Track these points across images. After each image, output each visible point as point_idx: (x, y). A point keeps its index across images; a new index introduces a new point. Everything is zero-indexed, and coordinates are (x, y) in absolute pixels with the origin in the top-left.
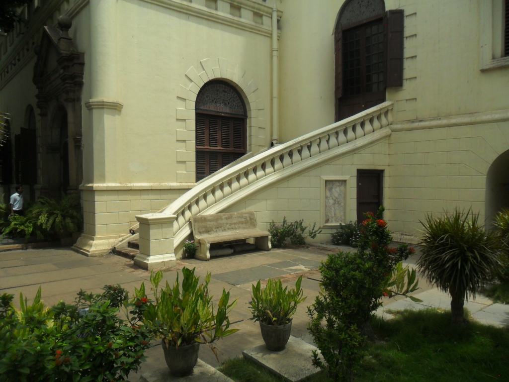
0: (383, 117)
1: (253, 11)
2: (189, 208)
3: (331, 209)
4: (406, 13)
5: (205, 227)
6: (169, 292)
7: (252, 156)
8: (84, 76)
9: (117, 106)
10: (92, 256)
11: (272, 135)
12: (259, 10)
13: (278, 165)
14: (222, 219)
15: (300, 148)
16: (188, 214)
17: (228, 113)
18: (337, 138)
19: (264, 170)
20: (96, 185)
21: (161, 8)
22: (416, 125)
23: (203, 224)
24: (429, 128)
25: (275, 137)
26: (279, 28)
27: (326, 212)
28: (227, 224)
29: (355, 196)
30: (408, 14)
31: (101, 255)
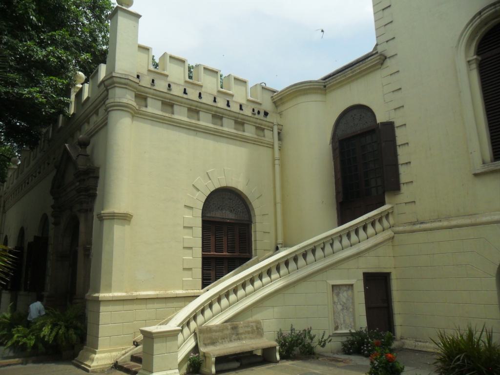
2: (195, 318)
4: (396, 125)
8: (98, 188)
9: (127, 217)
11: (276, 239)
13: (283, 270)
17: (234, 220)
18: (341, 242)
22: (417, 227)
24: (431, 230)
26: (280, 139)
27: (334, 319)
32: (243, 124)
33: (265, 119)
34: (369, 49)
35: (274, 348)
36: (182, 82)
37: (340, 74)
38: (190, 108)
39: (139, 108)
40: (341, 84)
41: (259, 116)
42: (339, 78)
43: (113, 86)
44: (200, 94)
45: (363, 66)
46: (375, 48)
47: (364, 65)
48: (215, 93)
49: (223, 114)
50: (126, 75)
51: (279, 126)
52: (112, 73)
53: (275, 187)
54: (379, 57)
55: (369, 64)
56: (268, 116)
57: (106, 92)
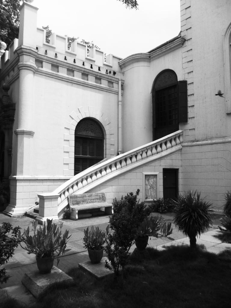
0: (177, 140)
1: (108, 81)
2: (68, 190)
3: (149, 191)
4: (188, 83)
5: (76, 201)
6: (41, 231)
7: (107, 160)
8: (15, 116)
9: (31, 133)
10: (13, 217)
11: (118, 149)
12: (111, 80)
13: (119, 166)
14: (86, 197)
15: (131, 156)
16: (67, 194)
17: (94, 137)
18: (151, 151)
19: (111, 169)
20: (18, 177)
21: (58, 80)
22: (195, 143)
23: (75, 199)
25: (120, 150)
26: (122, 89)
27: (145, 193)
28: (89, 199)
29: (162, 184)
30: (189, 83)
31: (19, 217)
32: (100, 79)
33: (114, 76)
34: (176, 35)
35: (111, 207)
36: (64, 52)
37: (159, 49)
38: (69, 69)
39: (38, 68)
40: (159, 56)
41: (110, 74)
42: (158, 52)
43: (22, 54)
44: (75, 60)
45: (172, 45)
46: (180, 34)
47: (173, 44)
48: (84, 60)
49: (88, 73)
50: (29, 47)
51: (122, 81)
52: (21, 46)
53: (118, 118)
54: (181, 40)
55: (176, 43)
56: (116, 75)
57: (18, 57)
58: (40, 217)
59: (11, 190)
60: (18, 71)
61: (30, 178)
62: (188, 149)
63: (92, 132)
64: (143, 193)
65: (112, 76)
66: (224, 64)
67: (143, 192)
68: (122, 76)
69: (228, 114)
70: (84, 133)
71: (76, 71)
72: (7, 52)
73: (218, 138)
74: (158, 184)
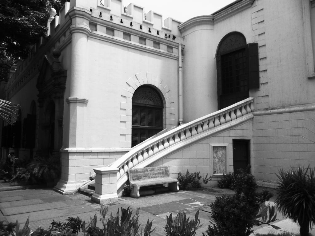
1: (167, 45)
2: (127, 164)
3: (217, 165)
4: (259, 45)
5: (137, 176)
6: (112, 221)
7: (167, 131)
8: (66, 83)
10: (66, 194)
12: (171, 44)
13: (183, 137)
15: (196, 126)
16: (126, 168)
17: (152, 105)
18: (219, 120)
19: (174, 140)
20: (70, 149)
21: (113, 44)
22: (269, 111)
23: (136, 174)
24: (278, 113)
26: (183, 54)
27: (213, 167)
28: (151, 174)
30: (260, 46)
31: (71, 194)
33: (173, 41)
35: (176, 183)
36: (120, 15)
37: (224, 11)
38: (125, 32)
39: (92, 31)
41: (170, 39)
42: (223, 14)
44: (131, 23)
47: (240, 4)
48: (141, 23)
49: (146, 37)
50: (83, 9)
56: (175, 39)
57: (70, 20)
58: (97, 195)
59: (62, 164)
60: (70, 35)
61: (84, 150)
62: (260, 118)
63: (150, 100)
64: (211, 167)
65: (172, 41)
66: (304, 23)
67: (211, 166)
68: (182, 41)
69: (310, 79)
70: (142, 102)
71: (133, 35)
72: (57, 17)
73: (298, 106)
74: (228, 157)
